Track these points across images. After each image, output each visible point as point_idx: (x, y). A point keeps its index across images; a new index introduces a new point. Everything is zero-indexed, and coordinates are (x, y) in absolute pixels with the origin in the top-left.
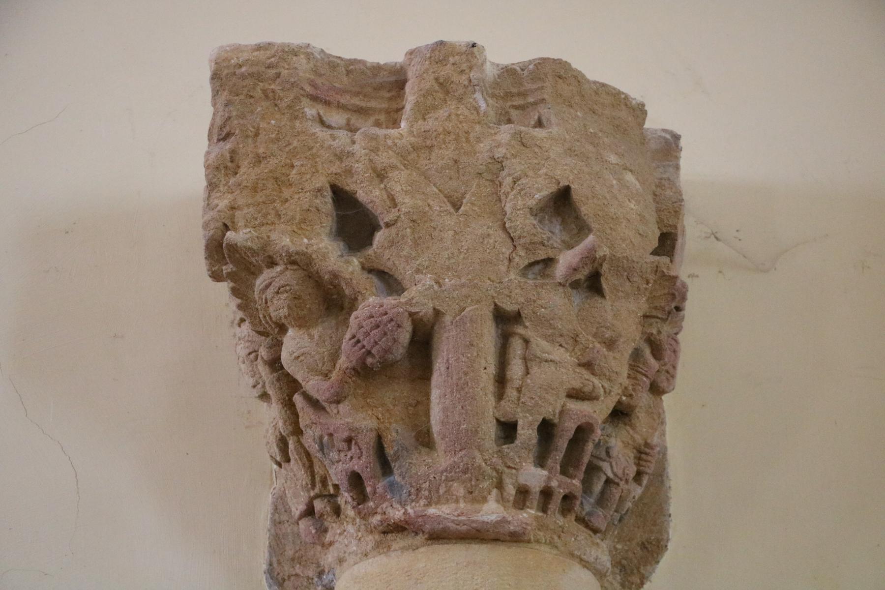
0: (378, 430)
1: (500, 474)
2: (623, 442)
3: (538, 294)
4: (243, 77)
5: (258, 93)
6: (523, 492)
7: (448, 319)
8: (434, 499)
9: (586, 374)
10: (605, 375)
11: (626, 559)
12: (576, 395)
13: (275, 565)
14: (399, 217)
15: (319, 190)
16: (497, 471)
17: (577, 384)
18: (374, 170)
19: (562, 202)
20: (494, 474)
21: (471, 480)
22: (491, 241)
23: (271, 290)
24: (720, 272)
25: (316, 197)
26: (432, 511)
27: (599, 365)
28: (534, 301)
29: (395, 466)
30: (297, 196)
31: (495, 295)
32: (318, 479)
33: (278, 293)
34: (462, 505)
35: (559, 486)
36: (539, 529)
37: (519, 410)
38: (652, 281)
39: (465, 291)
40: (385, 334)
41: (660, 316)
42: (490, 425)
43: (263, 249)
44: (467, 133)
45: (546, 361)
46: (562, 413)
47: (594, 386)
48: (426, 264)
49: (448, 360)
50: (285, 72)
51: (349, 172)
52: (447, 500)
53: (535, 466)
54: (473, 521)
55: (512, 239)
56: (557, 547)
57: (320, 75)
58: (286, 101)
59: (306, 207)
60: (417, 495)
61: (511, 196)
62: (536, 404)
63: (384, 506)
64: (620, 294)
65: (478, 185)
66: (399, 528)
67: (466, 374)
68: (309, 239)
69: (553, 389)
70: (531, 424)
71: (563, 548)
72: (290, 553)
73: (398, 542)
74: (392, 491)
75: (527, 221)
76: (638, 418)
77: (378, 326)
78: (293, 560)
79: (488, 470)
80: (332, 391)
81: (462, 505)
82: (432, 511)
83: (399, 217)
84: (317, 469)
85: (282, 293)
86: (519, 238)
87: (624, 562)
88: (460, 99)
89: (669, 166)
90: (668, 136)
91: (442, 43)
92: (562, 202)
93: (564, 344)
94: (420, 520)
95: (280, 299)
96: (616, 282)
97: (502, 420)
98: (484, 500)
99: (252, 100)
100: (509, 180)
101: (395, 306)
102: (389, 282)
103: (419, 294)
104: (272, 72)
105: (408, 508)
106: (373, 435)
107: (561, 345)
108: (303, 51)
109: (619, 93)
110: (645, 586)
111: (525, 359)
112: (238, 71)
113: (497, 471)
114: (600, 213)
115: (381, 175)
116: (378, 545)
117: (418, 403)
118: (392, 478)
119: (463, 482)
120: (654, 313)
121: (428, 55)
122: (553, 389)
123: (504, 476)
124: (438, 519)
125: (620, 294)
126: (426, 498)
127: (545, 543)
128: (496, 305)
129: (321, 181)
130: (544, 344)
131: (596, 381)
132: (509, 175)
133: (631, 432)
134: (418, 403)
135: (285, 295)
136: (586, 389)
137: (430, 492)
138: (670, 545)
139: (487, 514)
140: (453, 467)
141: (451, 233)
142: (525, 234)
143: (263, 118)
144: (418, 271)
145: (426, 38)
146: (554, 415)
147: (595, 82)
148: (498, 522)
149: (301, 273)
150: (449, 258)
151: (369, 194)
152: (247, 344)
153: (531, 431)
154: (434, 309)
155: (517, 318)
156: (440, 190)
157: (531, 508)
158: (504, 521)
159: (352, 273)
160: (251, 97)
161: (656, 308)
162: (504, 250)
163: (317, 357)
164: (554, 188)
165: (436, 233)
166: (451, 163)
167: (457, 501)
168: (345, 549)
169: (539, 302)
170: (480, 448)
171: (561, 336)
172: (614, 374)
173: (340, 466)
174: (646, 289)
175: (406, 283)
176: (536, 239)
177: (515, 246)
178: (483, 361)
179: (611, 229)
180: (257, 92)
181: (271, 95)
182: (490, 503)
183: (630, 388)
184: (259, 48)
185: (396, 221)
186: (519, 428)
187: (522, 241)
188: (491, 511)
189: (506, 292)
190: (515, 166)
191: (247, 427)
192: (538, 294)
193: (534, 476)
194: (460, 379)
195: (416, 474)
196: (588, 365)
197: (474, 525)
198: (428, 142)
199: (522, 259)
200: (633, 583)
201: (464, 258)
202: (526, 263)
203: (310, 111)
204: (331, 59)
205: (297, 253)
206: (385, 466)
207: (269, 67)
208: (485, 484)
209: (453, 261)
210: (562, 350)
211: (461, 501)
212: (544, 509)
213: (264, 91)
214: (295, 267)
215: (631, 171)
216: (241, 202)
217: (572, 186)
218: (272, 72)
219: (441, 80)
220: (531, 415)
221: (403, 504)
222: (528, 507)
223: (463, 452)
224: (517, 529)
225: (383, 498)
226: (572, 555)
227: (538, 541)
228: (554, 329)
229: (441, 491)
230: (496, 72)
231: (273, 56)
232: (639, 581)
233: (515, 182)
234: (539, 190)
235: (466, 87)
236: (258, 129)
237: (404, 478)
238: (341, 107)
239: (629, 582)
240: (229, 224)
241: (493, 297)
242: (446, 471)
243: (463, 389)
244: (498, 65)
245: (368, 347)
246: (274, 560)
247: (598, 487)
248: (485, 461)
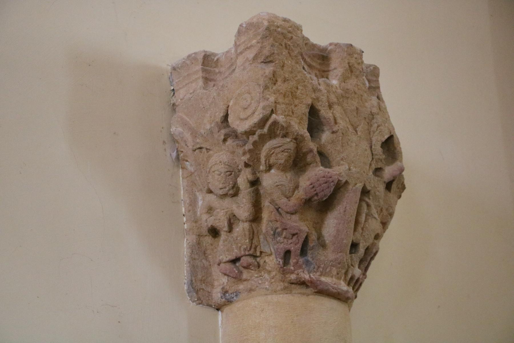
0: (308, 233)
4: (279, 33)
7: (350, 187)
13: (194, 281)
14: (338, 130)
23: (281, 149)
26: (323, 279)
29: (309, 252)
32: (253, 246)
33: (282, 151)
34: (334, 279)
49: (346, 207)
50: (294, 37)
51: (318, 99)
54: (339, 289)
59: (303, 112)
61: (376, 134)
63: (300, 271)
66: (303, 283)
72: (200, 277)
73: (298, 289)
74: (306, 265)
77: (326, 183)
78: (201, 280)
80: (295, 208)
82: (323, 279)
83: (338, 130)
84: (254, 241)
85: (285, 152)
88: (357, 77)
91: (351, 45)
94: (318, 282)
95: (283, 154)
100: (376, 125)
102: (324, 158)
103: (339, 171)
104: (290, 35)
105: (311, 275)
106: (306, 234)
111: (367, 215)
115: (330, 106)
116: (285, 288)
117: (318, 223)
118: (306, 258)
121: (346, 49)
124: (326, 284)
126: (321, 272)
128: (365, 184)
132: (377, 123)
134: (318, 223)
135: (286, 154)
140: (336, 259)
144: (342, 159)
145: (344, 40)
149: (295, 145)
151: (324, 112)
152: (226, 166)
155: (368, 192)
163: (288, 188)
165: (349, 143)
168: (258, 285)
169: (378, 189)
173: (282, 246)
175: (334, 163)
180: (279, 44)
181: (288, 47)
184: (285, 20)
187: (377, 157)
191: (173, 202)
195: (320, 259)
197: (339, 291)
198: (347, 95)
206: (303, 252)
207: (289, 32)
211: (334, 277)
216: (280, 100)
218: (290, 35)
219: (351, 65)
221: (309, 273)
223: (341, 254)
225: (300, 267)
229: (328, 270)
231: (291, 27)
235: (360, 72)
236: (284, 63)
237: (313, 260)
238: (305, 61)
245: (318, 191)
246: (193, 278)
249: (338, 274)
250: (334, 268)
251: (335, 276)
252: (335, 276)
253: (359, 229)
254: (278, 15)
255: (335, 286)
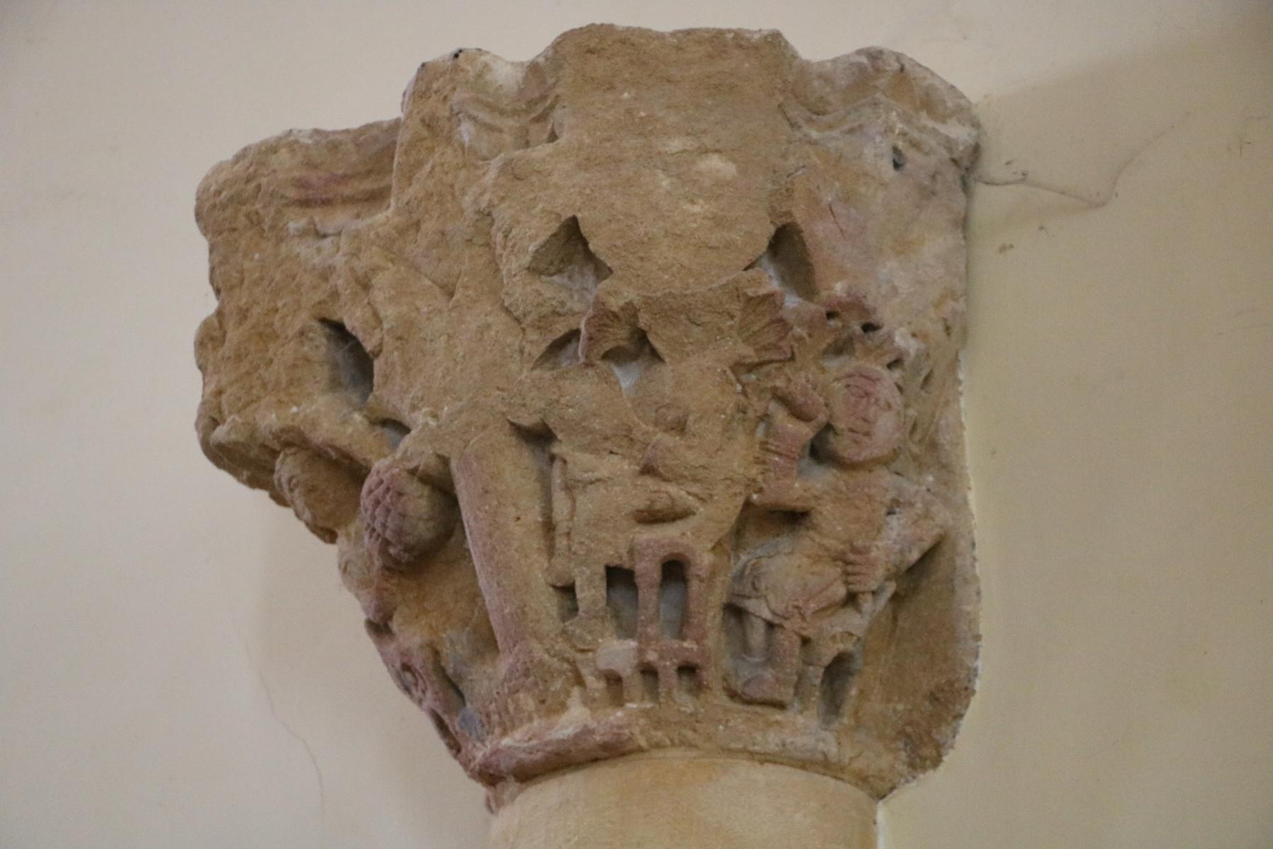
1: (573, 663)
2: (808, 557)
3: (559, 388)
4: (224, 207)
5: (242, 221)
6: (614, 680)
8: (508, 724)
9: (649, 482)
10: (683, 476)
11: (910, 723)
12: (651, 517)
14: (382, 339)
15: (302, 333)
16: (567, 661)
17: (641, 503)
18: (357, 280)
19: (571, 244)
20: (566, 666)
21: (536, 684)
22: (493, 333)
24: (1041, 228)
25: (302, 344)
26: (506, 741)
27: (665, 466)
28: (557, 401)
30: (281, 350)
31: (505, 409)
35: (661, 658)
36: (655, 728)
37: (572, 565)
38: (738, 314)
39: (464, 417)
40: (388, 511)
41: (775, 357)
42: (543, 598)
43: (252, 436)
44: (452, 186)
45: (592, 483)
46: (631, 552)
47: (671, 497)
48: (420, 394)
50: (264, 181)
52: (521, 721)
53: (619, 637)
54: (547, 744)
55: (517, 320)
56: (696, 746)
57: (316, 167)
58: (268, 222)
60: (489, 723)
62: (589, 551)
64: (689, 348)
65: (471, 258)
67: (490, 535)
68: (298, 405)
69: (607, 521)
70: (590, 581)
71: (708, 745)
75: (529, 289)
76: (821, 513)
79: (555, 663)
81: (536, 723)
83: (382, 339)
86: (525, 315)
87: (909, 729)
89: (864, 105)
90: (864, 60)
92: (571, 244)
93: (615, 449)
96: (675, 333)
97: (559, 584)
98: (563, 707)
99: (236, 234)
100: (500, 236)
101: (390, 467)
107: (611, 452)
108: (288, 142)
109: (720, 33)
110: (945, 758)
112: (218, 200)
113: (567, 661)
114: (619, 243)
119: (529, 690)
120: (766, 356)
122: (607, 521)
123: (579, 666)
125: (689, 348)
127: (673, 744)
128: (512, 424)
129: (303, 319)
130: (586, 458)
131: (672, 489)
133: (817, 539)
136: (658, 506)
137: (500, 716)
138: (978, 685)
139: (563, 727)
140: (511, 671)
141: (444, 338)
142: (529, 309)
143: (245, 255)
146: (620, 557)
147: (674, 34)
148: (577, 736)
150: (444, 377)
153: (593, 591)
154: (439, 456)
156: (434, 282)
157: (631, 701)
158: (586, 731)
159: (351, 435)
160: (234, 230)
161: (765, 348)
162: (509, 340)
164: (554, 227)
166: (437, 238)
167: (530, 719)
169: (563, 401)
170: (537, 636)
171: (606, 438)
172: (701, 470)
174: (731, 327)
176: (544, 310)
177: (523, 330)
178: (512, 511)
179: (642, 259)
182: (572, 709)
183: (760, 478)
185: (381, 345)
186: (578, 590)
188: (573, 720)
189: (518, 401)
190: (503, 214)
192: (559, 388)
193: (617, 652)
194: (485, 545)
196: (648, 470)
197: (549, 749)
199: (537, 343)
200: (926, 759)
201: (462, 370)
202: (544, 346)
203: (296, 222)
204: (331, 137)
205: (283, 431)
208: (557, 685)
209: (448, 378)
210: (615, 459)
211: (535, 716)
212: (654, 694)
213: (248, 216)
214: (293, 450)
215: (717, 151)
217: (579, 216)
220: (587, 566)
222: (627, 701)
224: (606, 739)
226: (729, 752)
227: (658, 746)
228: (590, 432)
229: (511, 709)
230: (520, 75)
232: (934, 753)
233: (506, 237)
234: (532, 239)
239: (921, 757)
240: (216, 416)
241: (503, 414)
242: (505, 680)
243: (492, 558)
244: (522, 64)
247: (757, 636)
248: (547, 651)
249: (543, 702)
250: (521, 695)
251: (538, 711)
252: (538, 711)
253: (561, 543)
254: (329, 126)
255: (534, 742)
